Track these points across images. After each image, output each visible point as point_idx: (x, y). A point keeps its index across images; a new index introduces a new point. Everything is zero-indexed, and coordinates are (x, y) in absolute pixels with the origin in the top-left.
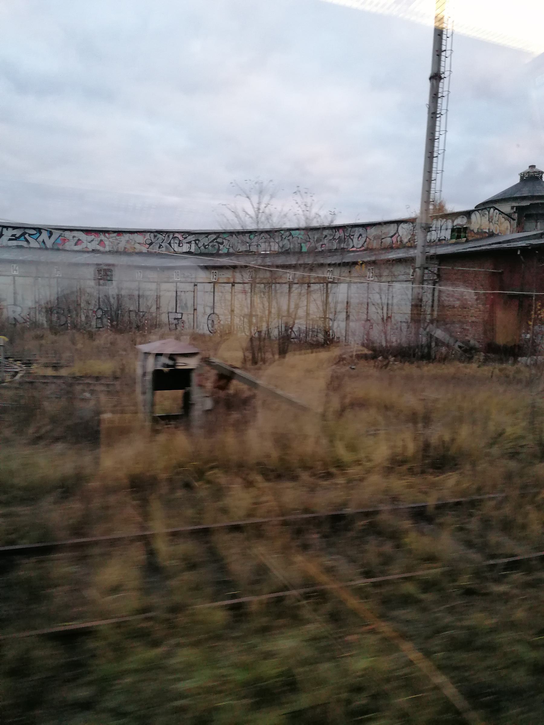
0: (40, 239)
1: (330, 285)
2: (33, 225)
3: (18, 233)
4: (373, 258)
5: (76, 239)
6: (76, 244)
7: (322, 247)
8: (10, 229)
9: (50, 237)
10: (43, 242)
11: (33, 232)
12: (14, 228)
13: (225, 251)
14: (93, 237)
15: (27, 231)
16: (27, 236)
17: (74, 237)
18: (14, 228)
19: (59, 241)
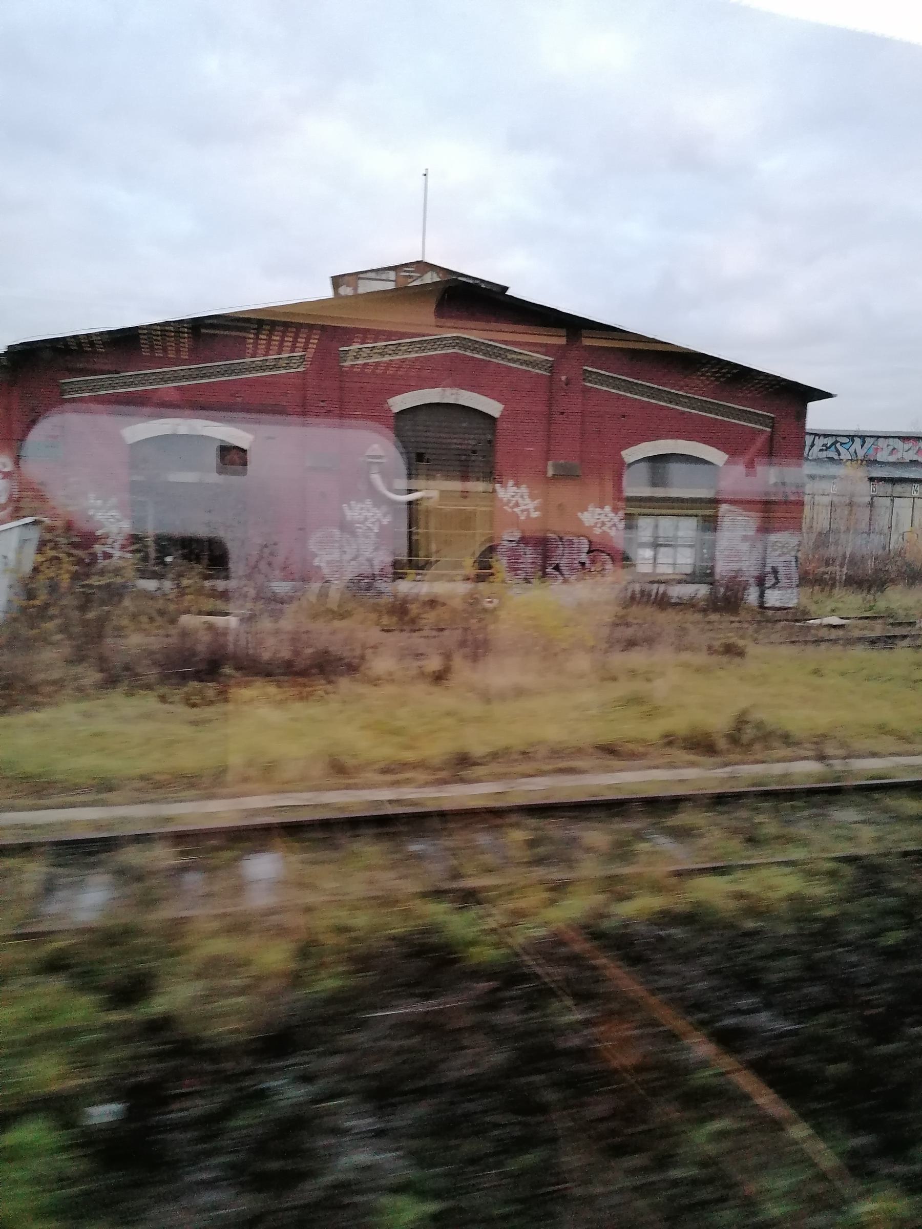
0: (852, 450)
1: (896, 500)
2: (214, 419)
3: (829, 441)
4: (221, 911)
5: (891, 448)
6: (891, 453)
7: (610, 528)
8: (822, 438)
9: (862, 446)
10: (855, 452)
11: (846, 440)
12: (826, 436)
13: (814, 457)
14: (911, 445)
15: (838, 439)
16: (838, 445)
17: (888, 445)
18: (826, 436)
19: (871, 452)
